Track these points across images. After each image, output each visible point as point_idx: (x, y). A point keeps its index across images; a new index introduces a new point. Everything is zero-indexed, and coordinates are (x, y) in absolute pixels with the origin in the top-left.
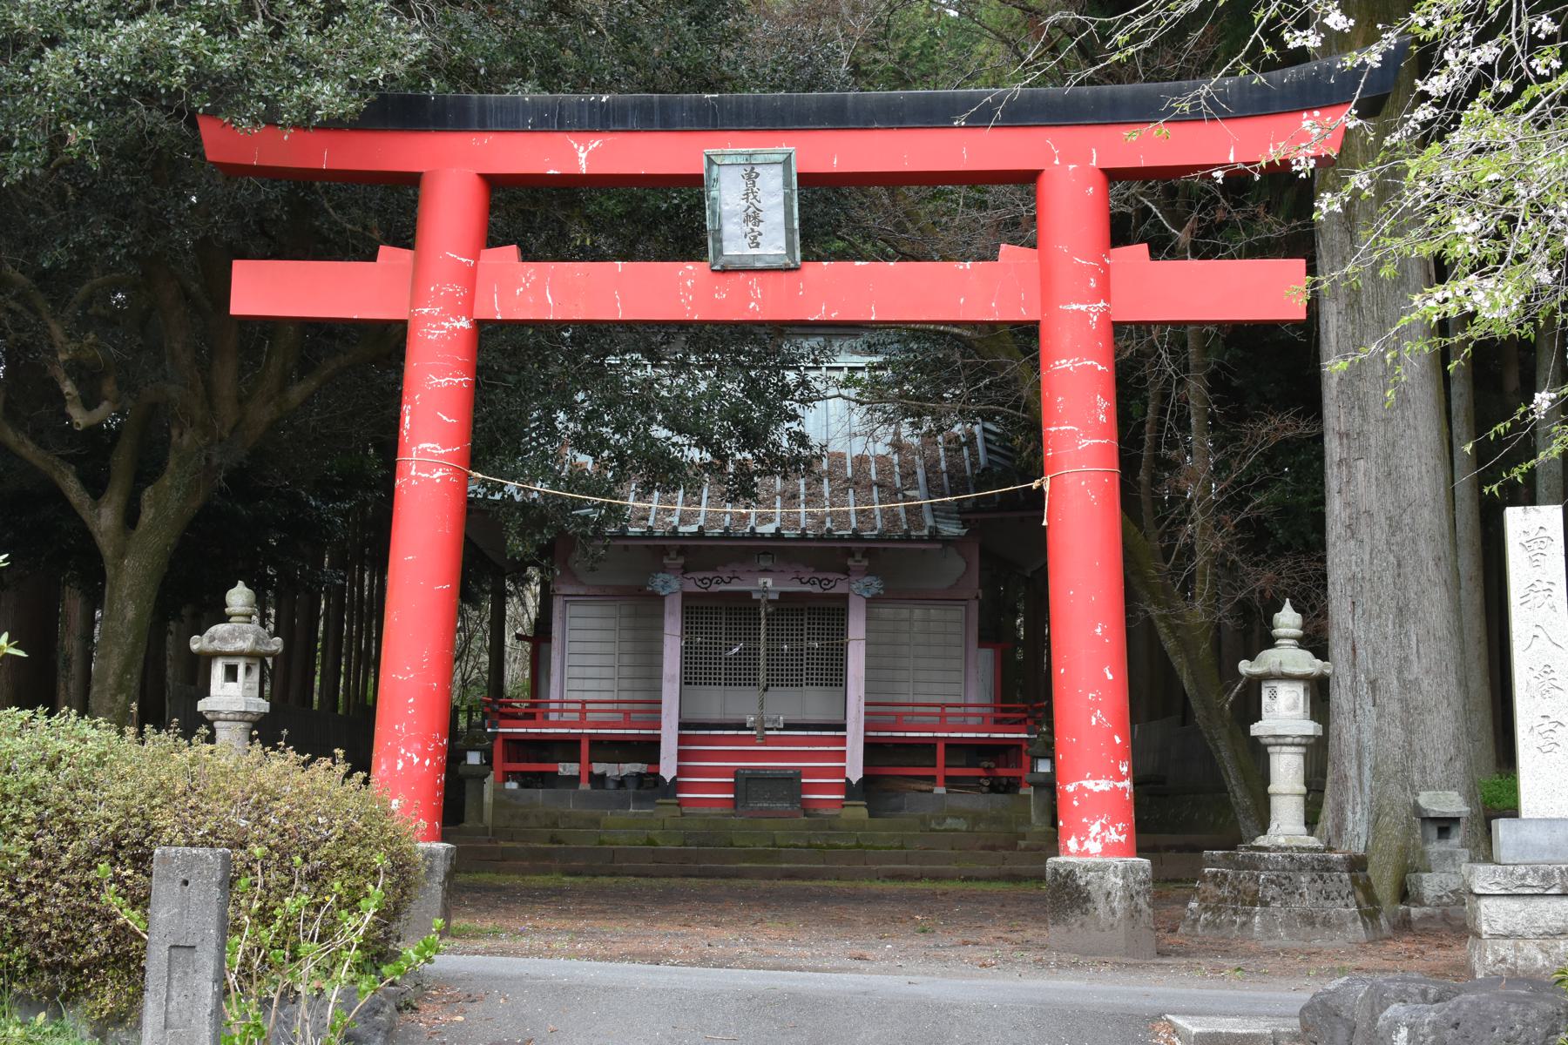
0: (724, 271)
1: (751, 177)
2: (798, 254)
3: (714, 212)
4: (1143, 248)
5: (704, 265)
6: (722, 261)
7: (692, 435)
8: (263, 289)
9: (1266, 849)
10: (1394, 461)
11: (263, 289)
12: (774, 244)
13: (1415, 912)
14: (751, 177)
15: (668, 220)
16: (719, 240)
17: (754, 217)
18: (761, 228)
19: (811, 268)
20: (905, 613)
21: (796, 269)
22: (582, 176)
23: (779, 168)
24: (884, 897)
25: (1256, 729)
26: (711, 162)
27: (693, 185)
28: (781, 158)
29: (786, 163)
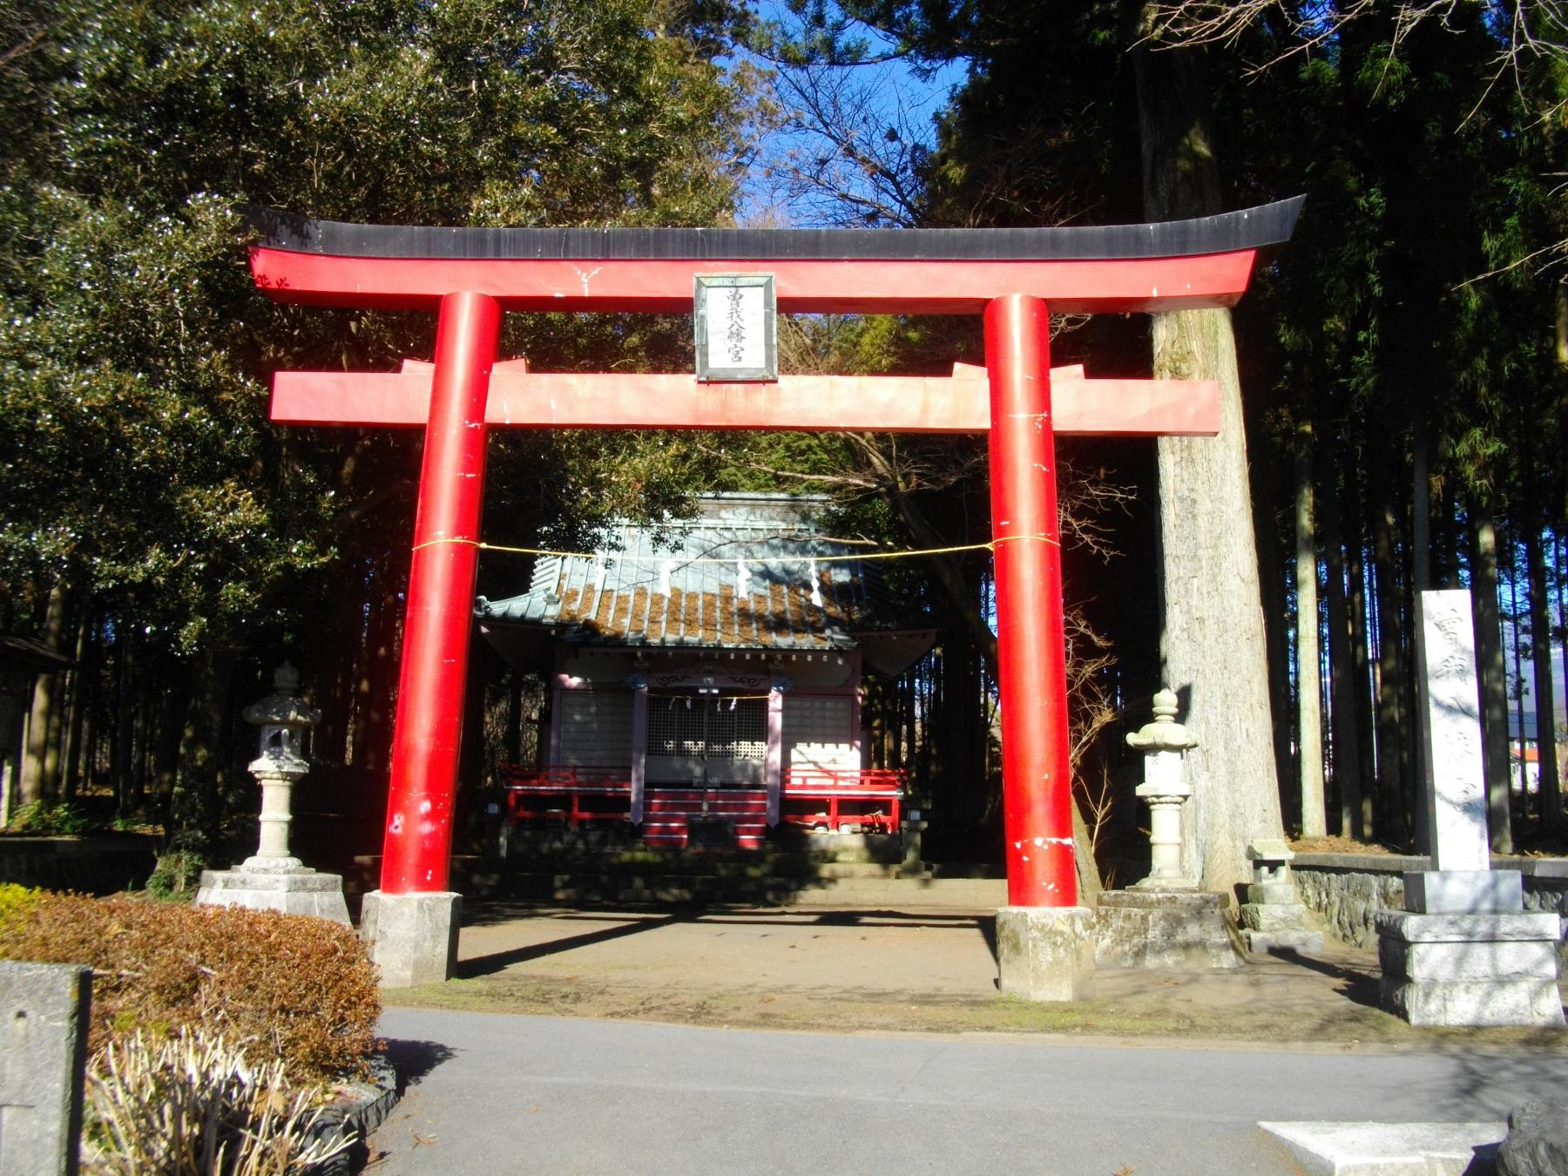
0: (709, 382)
1: (736, 298)
2: (776, 367)
3: (702, 329)
4: (1079, 368)
5: (694, 377)
6: (707, 373)
7: (726, 234)
8: (307, 396)
9: (1148, 891)
10: (1220, 579)
11: (307, 396)
12: (754, 358)
13: (1255, 936)
14: (736, 298)
15: (662, 337)
16: (705, 355)
17: (736, 334)
18: (743, 344)
19: (785, 381)
20: (807, 704)
21: (775, 381)
22: (584, 299)
23: (762, 290)
24: (914, 1000)
25: (1140, 790)
26: (700, 284)
27: (682, 308)
28: (762, 281)
29: (767, 286)
